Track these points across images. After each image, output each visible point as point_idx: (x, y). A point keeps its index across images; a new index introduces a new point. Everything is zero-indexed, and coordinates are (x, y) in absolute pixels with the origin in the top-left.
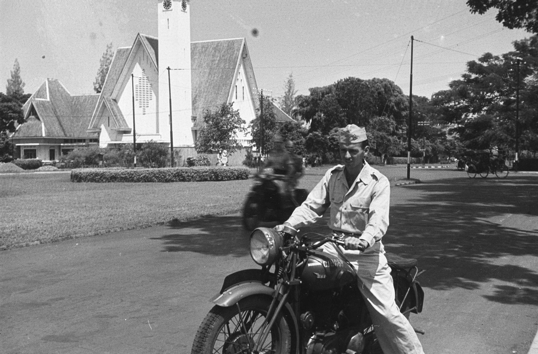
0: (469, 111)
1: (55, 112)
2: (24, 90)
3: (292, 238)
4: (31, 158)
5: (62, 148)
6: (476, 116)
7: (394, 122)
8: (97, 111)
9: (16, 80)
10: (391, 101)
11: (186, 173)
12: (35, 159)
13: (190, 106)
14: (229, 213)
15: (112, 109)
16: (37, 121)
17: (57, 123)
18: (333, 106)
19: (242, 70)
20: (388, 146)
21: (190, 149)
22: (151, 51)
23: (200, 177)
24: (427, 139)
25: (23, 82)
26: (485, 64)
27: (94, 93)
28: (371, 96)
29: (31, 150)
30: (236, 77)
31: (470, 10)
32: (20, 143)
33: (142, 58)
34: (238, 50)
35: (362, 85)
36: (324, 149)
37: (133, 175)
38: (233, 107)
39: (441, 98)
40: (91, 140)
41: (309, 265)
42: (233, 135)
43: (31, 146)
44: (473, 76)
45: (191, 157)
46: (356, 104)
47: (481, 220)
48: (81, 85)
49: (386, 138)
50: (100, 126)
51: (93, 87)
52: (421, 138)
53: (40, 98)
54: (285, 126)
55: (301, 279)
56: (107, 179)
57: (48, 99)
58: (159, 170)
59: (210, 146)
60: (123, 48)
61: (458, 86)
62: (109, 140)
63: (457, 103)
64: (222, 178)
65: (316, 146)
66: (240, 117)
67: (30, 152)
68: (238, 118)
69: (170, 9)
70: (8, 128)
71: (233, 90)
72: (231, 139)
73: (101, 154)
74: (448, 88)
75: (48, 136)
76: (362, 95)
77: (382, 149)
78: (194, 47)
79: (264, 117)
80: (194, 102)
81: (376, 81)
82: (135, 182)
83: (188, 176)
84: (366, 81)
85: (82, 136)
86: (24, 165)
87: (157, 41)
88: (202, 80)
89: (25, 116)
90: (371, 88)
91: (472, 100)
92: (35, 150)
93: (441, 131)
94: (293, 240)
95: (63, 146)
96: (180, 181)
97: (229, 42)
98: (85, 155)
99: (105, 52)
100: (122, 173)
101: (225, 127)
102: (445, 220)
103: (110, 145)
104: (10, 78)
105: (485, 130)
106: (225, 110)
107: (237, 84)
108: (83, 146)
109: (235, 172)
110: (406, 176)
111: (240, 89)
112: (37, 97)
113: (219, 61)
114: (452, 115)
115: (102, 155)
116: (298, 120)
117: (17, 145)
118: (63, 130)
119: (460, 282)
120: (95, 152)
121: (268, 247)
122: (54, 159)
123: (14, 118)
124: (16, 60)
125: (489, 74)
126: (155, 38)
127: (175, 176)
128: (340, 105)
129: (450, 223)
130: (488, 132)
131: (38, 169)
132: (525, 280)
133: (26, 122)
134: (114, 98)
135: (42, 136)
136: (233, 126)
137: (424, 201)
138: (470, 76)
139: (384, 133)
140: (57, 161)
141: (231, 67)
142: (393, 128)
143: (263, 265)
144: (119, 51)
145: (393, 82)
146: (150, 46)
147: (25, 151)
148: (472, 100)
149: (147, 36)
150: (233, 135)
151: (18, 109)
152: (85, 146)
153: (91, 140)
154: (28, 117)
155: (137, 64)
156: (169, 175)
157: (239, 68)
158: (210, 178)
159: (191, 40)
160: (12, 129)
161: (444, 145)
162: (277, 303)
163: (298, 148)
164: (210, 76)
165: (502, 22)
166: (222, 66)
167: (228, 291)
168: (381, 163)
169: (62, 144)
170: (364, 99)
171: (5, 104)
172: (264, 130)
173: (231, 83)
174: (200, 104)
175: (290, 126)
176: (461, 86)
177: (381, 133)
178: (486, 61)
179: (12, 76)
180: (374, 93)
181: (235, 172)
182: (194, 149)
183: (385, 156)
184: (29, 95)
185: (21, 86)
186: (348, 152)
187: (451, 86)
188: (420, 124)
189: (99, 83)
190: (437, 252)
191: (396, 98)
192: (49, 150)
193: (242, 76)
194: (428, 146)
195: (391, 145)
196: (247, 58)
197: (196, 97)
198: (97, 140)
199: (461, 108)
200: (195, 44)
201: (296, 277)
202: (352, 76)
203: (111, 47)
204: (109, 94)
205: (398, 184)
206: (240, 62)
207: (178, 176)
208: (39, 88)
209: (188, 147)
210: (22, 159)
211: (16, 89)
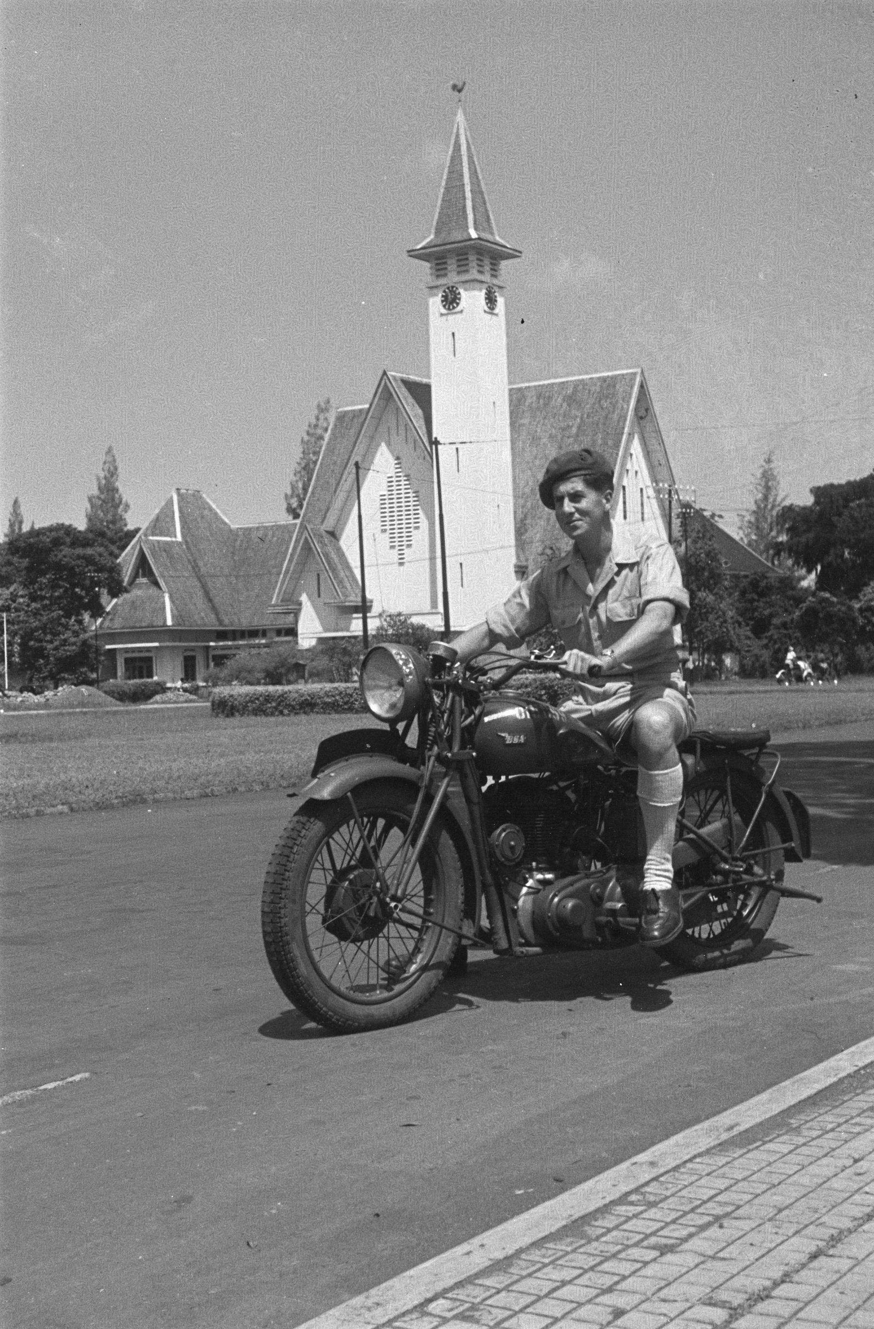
1: (195, 568)
2: (128, 520)
3: (448, 664)
4: (141, 677)
5: (212, 653)
8: (290, 561)
9: (108, 498)
12: (149, 680)
15: (326, 555)
16: (153, 591)
17: (200, 593)
19: (636, 447)
22: (414, 410)
25: (124, 500)
27: (286, 519)
29: (141, 659)
30: (623, 464)
32: (114, 643)
33: (393, 432)
34: (626, 399)
36: (848, 635)
37: (351, 696)
40: (279, 632)
41: (486, 719)
43: (140, 650)
48: (251, 502)
50: (300, 595)
51: (285, 506)
53: (161, 535)
54: (751, 583)
55: (473, 749)
56: (293, 708)
57: (179, 538)
60: (349, 408)
62: (320, 629)
65: (825, 628)
67: (138, 664)
69: (458, 309)
70: (86, 607)
73: (301, 662)
75: (180, 625)
78: (517, 399)
79: (693, 560)
82: (357, 712)
85: (257, 623)
86: (125, 693)
87: (427, 388)
89: (126, 580)
92: (150, 659)
94: (451, 668)
95: (215, 648)
97: (604, 380)
98: (263, 666)
99: (314, 421)
100: (327, 694)
103: (321, 640)
104: (95, 492)
107: (625, 483)
108: (259, 646)
112: (153, 534)
113: (579, 428)
115: (304, 666)
116: (773, 563)
117: (108, 647)
118: (214, 609)
120: (286, 659)
121: (401, 683)
122: (194, 679)
123: (98, 584)
124: (110, 450)
126: (425, 381)
131: (152, 701)
133: (126, 591)
134: (330, 529)
135: (165, 625)
140: (201, 684)
143: (393, 722)
144: (341, 418)
146: (411, 400)
147: (127, 660)
151: (106, 561)
152: (266, 646)
153: (279, 632)
154: (132, 582)
155: (383, 448)
157: (629, 441)
159: (510, 383)
160: (97, 610)
162: (429, 799)
163: (785, 636)
167: (326, 772)
169: (212, 644)
171: (80, 551)
175: (763, 584)
179: (99, 488)
184: (137, 530)
185: (120, 510)
186: (566, 501)
189: (298, 496)
192: (182, 658)
196: (648, 418)
198: (292, 632)
201: (463, 747)
203: (327, 410)
204: (319, 520)
208: (157, 511)
210: (121, 680)
211: (110, 517)
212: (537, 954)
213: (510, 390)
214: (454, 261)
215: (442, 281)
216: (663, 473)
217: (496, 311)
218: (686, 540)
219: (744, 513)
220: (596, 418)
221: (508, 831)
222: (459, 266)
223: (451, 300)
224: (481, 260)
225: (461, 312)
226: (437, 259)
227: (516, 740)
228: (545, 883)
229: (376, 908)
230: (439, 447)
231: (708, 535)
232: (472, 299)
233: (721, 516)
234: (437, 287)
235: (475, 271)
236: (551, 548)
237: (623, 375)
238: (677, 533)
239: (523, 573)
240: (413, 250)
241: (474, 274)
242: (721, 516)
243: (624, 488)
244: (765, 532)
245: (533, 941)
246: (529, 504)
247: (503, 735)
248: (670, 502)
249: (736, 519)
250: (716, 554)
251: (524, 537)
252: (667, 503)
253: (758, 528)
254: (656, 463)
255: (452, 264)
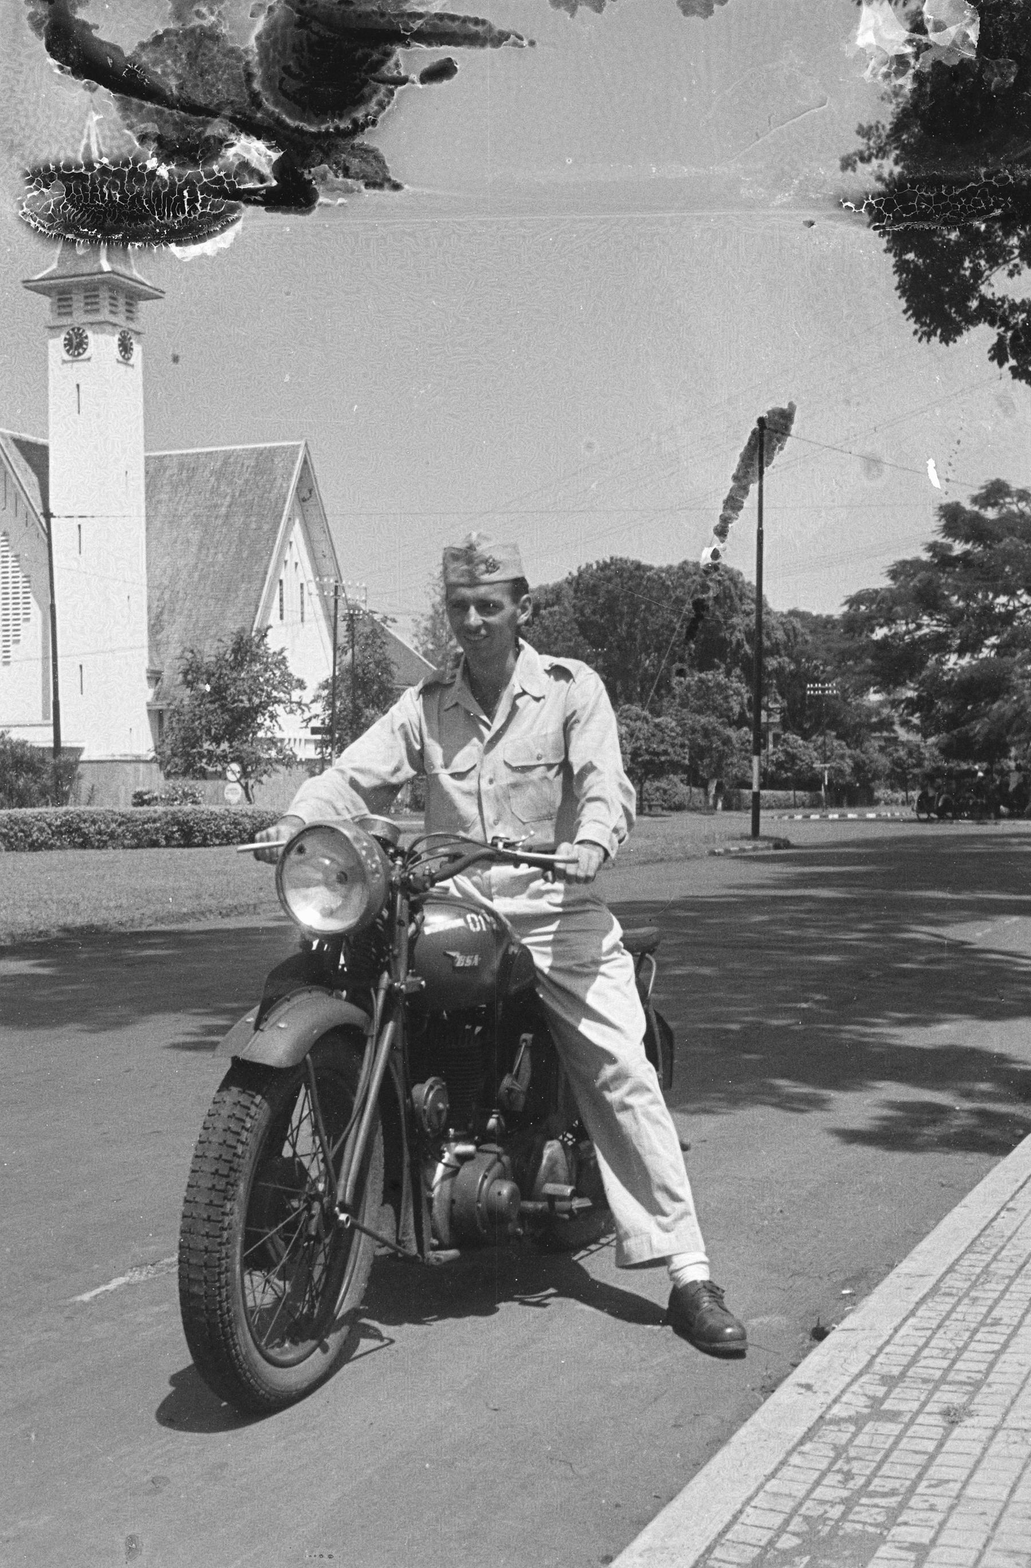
0: (946, 649)
6: (965, 661)
7: (743, 688)
10: (733, 627)
11: (94, 822)
13: (144, 638)
14: (160, 920)
18: (564, 640)
20: (723, 756)
21: (141, 766)
22: (29, 479)
23: (135, 835)
24: (838, 737)
26: (991, 514)
28: (673, 612)
30: (281, 553)
31: (915, 332)
35: (649, 579)
38: (267, 640)
39: (866, 609)
42: (268, 723)
44: (959, 548)
45: (144, 789)
46: (631, 637)
47: (922, 933)
49: (718, 734)
52: (823, 733)
58: (10, 816)
59: (201, 756)
61: (915, 574)
63: (912, 626)
64: (205, 839)
66: (291, 670)
68: (282, 675)
71: (270, 597)
72: (261, 734)
74: (885, 583)
76: (648, 608)
77: (709, 766)
78: (155, 472)
79: (360, 670)
80: (155, 627)
81: (690, 568)
83: (100, 832)
84: (661, 570)
87: (45, 449)
88: (181, 563)
90: (676, 588)
91: (956, 618)
93: (878, 714)
96: (75, 846)
97: (261, 452)
101: (244, 698)
102: (812, 933)
105: (994, 702)
106: (246, 649)
109: (246, 820)
110: (748, 830)
111: (291, 592)
114: (896, 664)
119: (773, 1090)
125: (1000, 541)
126: (41, 441)
127: (58, 833)
128: (585, 637)
129: (826, 940)
130: (1000, 707)
132: (984, 1086)
136: (269, 695)
137: (775, 887)
138: (950, 548)
139: (713, 719)
141: (266, 527)
142: (741, 704)
145: (740, 574)
146: (23, 463)
148: (956, 618)
149: (17, 434)
150: (268, 723)
156: (41, 830)
157: (288, 530)
158: (167, 838)
161: (891, 755)
164: (204, 552)
165: (1007, 366)
166: (238, 521)
168: (709, 808)
170: (654, 623)
172: (360, 709)
173: (266, 573)
174: (174, 633)
176: (921, 575)
177: (703, 720)
178: (994, 505)
180: (683, 602)
181: (246, 820)
182: (155, 766)
183: (719, 787)
187: (894, 574)
188: (812, 689)
190: (740, 1013)
191: (747, 621)
193: (298, 551)
194: (842, 757)
195: (732, 754)
197: (161, 613)
199: (923, 640)
200: (161, 459)
202: (619, 554)
205: (721, 850)
206: (293, 510)
207: (69, 833)
209: (138, 761)
212: (451, 1261)
213: (147, 458)
214: (81, 297)
215: (66, 321)
216: (328, 565)
217: (131, 362)
218: (353, 647)
219: (419, 618)
220: (250, 497)
221: (436, 1087)
222: (87, 304)
223: (76, 345)
224: (114, 299)
225: (89, 359)
226: (60, 293)
227: (469, 962)
228: (463, 1158)
229: (318, 1224)
230: (52, 520)
231: (379, 642)
232: (102, 345)
233: (394, 621)
234: (58, 327)
235: (106, 311)
236: (192, 651)
237: (283, 447)
238: (342, 640)
239: (157, 680)
240: (28, 281)
241: (105, 315)
242: (394, 621)
243: (281, 582)
244: (444, 640)
245: (446, 1241)
246: (166, 597)
247: (453, 954)
248: (336, 601)
249: (411, 625)
250: (388, 665)
251: (159, 637)
252: (332, 601)
253: (434, 635)
254: (320, 555)
255: (78, 301)
